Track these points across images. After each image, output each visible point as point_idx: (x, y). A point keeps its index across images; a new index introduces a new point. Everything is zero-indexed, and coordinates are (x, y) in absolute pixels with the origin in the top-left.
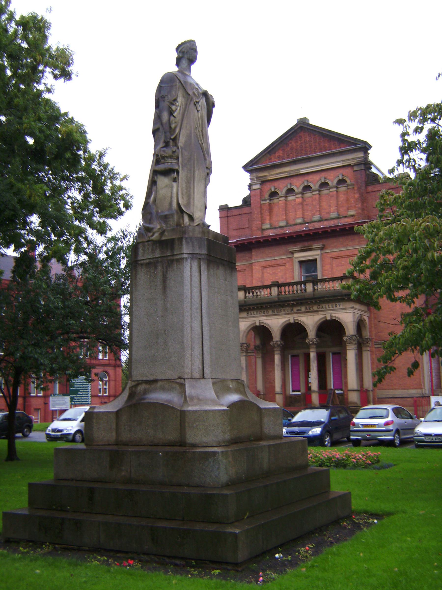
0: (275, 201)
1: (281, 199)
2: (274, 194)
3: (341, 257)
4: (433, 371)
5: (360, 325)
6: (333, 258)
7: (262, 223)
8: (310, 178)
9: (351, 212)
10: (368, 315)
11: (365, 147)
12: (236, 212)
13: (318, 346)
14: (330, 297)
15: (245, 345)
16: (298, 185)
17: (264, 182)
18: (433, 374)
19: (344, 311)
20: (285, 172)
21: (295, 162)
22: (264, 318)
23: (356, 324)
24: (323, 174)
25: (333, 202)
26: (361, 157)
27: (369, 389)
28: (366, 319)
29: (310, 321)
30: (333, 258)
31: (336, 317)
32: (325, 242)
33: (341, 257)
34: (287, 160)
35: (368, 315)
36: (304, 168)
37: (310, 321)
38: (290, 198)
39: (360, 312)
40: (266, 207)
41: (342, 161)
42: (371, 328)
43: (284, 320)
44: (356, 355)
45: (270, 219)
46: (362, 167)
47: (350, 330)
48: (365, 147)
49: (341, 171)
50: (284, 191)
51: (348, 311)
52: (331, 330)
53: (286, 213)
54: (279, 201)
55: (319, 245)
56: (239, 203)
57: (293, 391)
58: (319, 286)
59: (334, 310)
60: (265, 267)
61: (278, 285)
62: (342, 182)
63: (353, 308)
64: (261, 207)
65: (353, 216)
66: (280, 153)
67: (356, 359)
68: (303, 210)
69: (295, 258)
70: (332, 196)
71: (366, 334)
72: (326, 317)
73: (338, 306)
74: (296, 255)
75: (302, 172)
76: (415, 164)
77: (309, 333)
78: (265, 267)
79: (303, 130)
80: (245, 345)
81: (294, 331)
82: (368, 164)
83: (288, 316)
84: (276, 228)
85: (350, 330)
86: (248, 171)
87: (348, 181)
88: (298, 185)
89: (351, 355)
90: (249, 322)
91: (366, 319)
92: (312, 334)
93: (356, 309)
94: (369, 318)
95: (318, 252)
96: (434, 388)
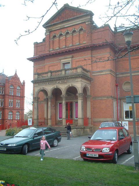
0: (55, 40)
1: (57, 38)
2: (55, 37)
3: (80, 61)
4: (118, 111)
5: (85, 90)
6: (76, 62)
7: (49, 49)
8: (68, 29)
9: (84, 42)
10: (90, 85)
11: (91, 14)
12: (40, 45)
13: (66, 98)
14: (72, 76)
15: (37, 98)
16: (64, 32)
17: (50, 32)
18: (118, 112)
19: (77, 82)
20: (59, 27)
21: (63, 22)
22: (45, 86)
23: (82, 89)
24: (74, 27)
25: (78, 38)
26: (89, 19)
27: (89, 118)
28: (89, 87)
29: (63, 87)
30: (76, 62)
31: (74, 85)
32: (73, 55)
33: (80, 61)
34: (59, 22)
35: (90, 85)
36: (66, 25)
37: (63, 87)
38: (61, 38)
39: (85, 84)
40: (51, 42)
41: (82, 20)
42: (91, 91)
43: (53, 87)
44: (82, 102)
45: (53, 47)
46: (90, 22)
47: (80, 91)
48: (91, 14)
49: (81, 25)
50: (59, 35)
51: (79, 82)
52: (72, 91)
53: (59, 44)
54: (57, 39)
55: (71, 56)
56: (41, 41)
57: (59, 118)
58: (67, 72)
59: (73, 82)
61: (51, 72)
62: (81, 30)
63: (81, 81)
64: (49, 41)
65: (85, 43)
66: (58, 19)
67: (82, 104)
68: (66, 42)
69: (61, 62)
70: (77, 36)
71: (89, 93)
72: (69, 85)
73: (75, 80)
74: (62, 61)
75: (66, 26)
76: (136, 85)
77: (63, 93)
79: (66, 8)
80: (37, 98)
81: (57, 92)
82: (92, 22)
83: (54, 85)
84: (55, 50)
85: (80, 91)
86: (45, 27)
87: (84, 29)
88: (64, 32)
89: (80, 102)
90: (38, 88)
91: (89, 87)
92: (64, 93)
93: (82, 81)
94: (91, 87)
95: (71, 59)
96: (119, 118)
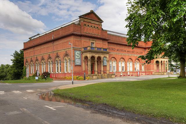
60: (84, 42)
74: (91, 41)
75: (92, 22)
78: (84, 42)
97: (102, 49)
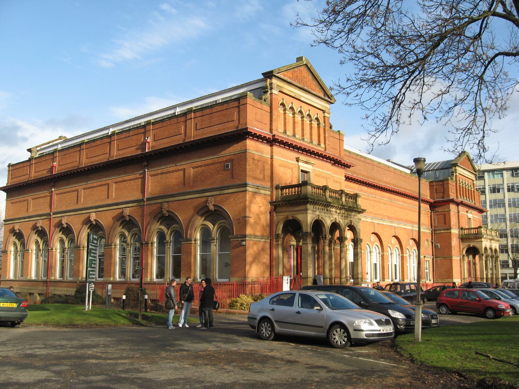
88: (288, 101)
97: (328, 193)
